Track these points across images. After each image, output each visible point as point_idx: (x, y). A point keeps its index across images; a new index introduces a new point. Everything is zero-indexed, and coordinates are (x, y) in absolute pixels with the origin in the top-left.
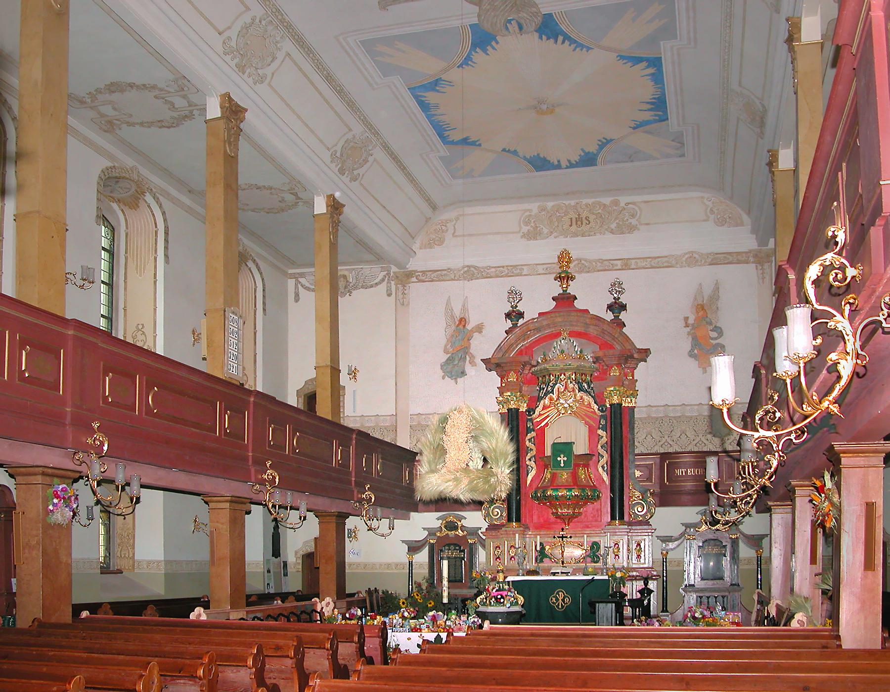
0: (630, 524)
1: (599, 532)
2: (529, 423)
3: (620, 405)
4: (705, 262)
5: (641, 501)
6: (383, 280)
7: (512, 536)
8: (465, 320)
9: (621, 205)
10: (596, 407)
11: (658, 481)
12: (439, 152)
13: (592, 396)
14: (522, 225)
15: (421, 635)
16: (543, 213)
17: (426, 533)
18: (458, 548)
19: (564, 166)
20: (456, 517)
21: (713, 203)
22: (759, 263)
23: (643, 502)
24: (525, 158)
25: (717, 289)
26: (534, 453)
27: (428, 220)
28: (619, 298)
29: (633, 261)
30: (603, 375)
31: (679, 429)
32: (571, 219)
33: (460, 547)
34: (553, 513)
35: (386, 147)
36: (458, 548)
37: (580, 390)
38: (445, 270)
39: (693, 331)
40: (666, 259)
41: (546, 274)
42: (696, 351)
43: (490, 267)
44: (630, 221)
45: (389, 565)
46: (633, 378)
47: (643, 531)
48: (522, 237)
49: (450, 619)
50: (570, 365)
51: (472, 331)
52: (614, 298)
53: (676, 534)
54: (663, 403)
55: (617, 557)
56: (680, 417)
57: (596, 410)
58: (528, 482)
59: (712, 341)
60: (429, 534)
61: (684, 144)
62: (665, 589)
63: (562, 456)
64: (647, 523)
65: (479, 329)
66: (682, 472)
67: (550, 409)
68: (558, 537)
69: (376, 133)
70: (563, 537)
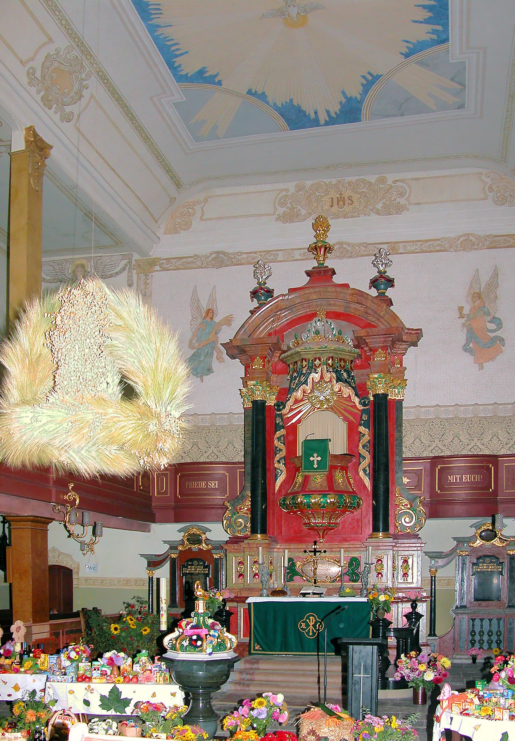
0: (396, 537)
1: (360, 546)
2: (278, 419)
3: (385, 395)
4: (482, 246)
5: (409, 511)
6: (124, 269)
7: (255, 549)
8: (213, 312)
9: (388, 183)
10: (356, 400)
11: (427, 489)
12: (173, 95)
13: (353, 387)
14: (277, 206)
15: (89, 686)
16: (301, 193)
17: (167, 547)
18: (202, 563)
19: (322, 122)
20: (200, 528)
21: (492, 180)
23: (411, 512)
24: (275, 107)
25: (495, 275)
26: (283, 453)
27: (173, 200)
28: (385, 272)
29: (401, 245)
30: (366, 363)
32: (332, 199)
33: (205, 563)
34: (305, 524)
35: (104, 79)
36: (202, 563)
37: (339, 380)
38: (191, 257)
40: (439, 242)
42: (471, 345)
43: (240, 252)
44: (398, 200)
45: (128, 581)
46: (401, 365)
47: (411, 545)
48: (277, 220)
49: (138, 663)
50: (326, 347)
51: (220, 324)
52: (379, 272)
53: (446, 549)
54: (434, 403)
55: (380, 575)
56: (452, 419)
57: (357, 404)
58: (277, 488)
59: (490, 334)
60: (171, 548)
61: (465, 87)
62: (432, 610)
63: (315, 455)
64: (416, 537)
66: (456, 479)
67: (303, 403)
68: (310, 551)
69: (86, 52)
70: (315, 551)
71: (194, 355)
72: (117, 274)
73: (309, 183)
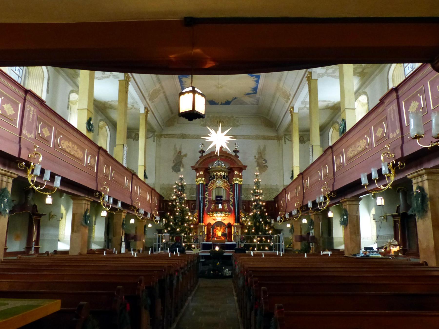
6: (152, 136)
29: (238, 137)
48: (201, 126)
54: (275, 184)
65: (185, 155)
71: (174, 165)
72: (150, 138)
73: (211, 116)
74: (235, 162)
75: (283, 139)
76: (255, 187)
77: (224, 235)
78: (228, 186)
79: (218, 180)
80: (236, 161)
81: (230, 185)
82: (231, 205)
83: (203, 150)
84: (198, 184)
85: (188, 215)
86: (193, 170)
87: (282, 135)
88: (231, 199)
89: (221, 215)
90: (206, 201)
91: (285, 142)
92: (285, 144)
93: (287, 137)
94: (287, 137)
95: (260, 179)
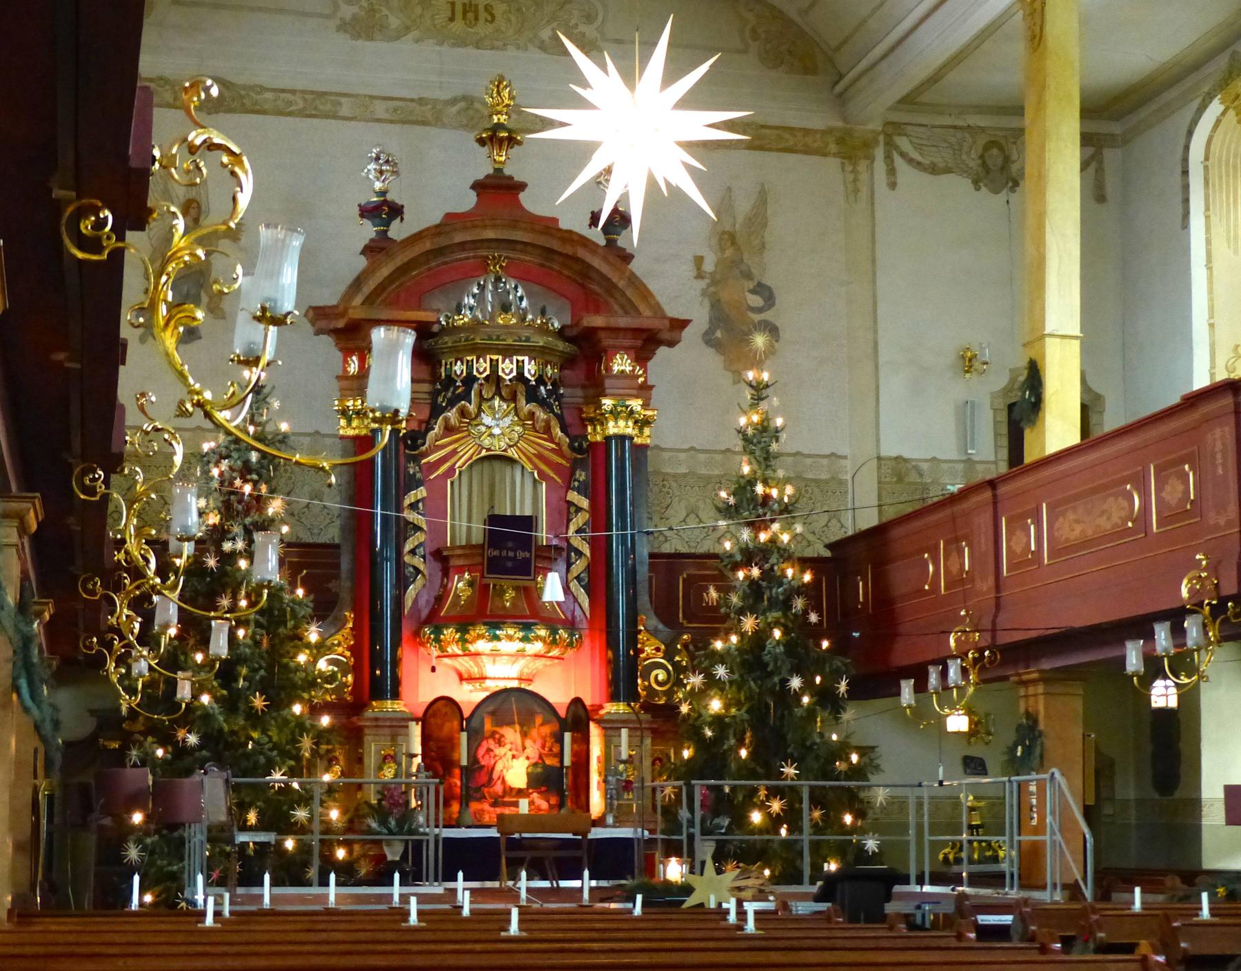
8: (199, 207)
22: (850, 158)
25: (762, 199)
31: (683, 504)
39: (712, 289)
41: (392, 122)
43: (261, 87)
50: (528, 340)
54: (686, 446)
56: (685, 475)
74: (611, 287)
75: (879, 153)
76: (750, 463)
77: (544, 779)
78: (558, 452)
79: (492, 408)
80: (621, 284)
81: (571, 446)
82: (578, 578)
83: (389, 197)
84: (351, 432)
85: (308, 646)
86: (318, 333)
87: (870, 127)
88: (577, 542)
89: (520, 645)
90: (413, 552)
91: (892, 171)
92: (893, 185)
93: (903, 143)
94: (903, 143)
95: (777, 414)
